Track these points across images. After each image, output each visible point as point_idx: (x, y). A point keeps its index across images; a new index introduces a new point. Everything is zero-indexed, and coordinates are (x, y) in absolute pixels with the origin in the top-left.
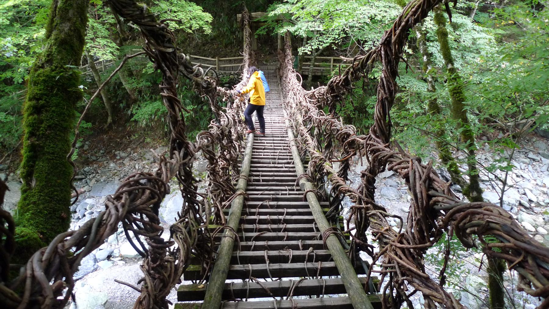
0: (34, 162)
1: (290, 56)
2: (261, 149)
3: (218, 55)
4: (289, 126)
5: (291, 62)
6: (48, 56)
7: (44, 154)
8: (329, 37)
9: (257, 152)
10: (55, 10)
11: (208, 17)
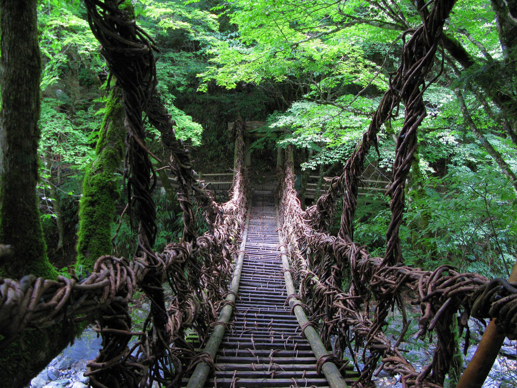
0: (89, 239)
1: (290, 174)
2: (251, 273)
3: (201, 169)
4: (284, 252)
5: (291, 182)
6: (100, 166)
7: (96, 235)
8: (337, 153)
9: (246, 276)
10: (105, 133)
11: (198, 128)
